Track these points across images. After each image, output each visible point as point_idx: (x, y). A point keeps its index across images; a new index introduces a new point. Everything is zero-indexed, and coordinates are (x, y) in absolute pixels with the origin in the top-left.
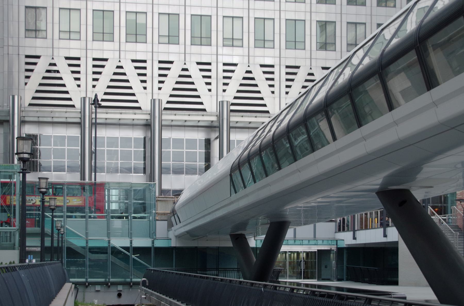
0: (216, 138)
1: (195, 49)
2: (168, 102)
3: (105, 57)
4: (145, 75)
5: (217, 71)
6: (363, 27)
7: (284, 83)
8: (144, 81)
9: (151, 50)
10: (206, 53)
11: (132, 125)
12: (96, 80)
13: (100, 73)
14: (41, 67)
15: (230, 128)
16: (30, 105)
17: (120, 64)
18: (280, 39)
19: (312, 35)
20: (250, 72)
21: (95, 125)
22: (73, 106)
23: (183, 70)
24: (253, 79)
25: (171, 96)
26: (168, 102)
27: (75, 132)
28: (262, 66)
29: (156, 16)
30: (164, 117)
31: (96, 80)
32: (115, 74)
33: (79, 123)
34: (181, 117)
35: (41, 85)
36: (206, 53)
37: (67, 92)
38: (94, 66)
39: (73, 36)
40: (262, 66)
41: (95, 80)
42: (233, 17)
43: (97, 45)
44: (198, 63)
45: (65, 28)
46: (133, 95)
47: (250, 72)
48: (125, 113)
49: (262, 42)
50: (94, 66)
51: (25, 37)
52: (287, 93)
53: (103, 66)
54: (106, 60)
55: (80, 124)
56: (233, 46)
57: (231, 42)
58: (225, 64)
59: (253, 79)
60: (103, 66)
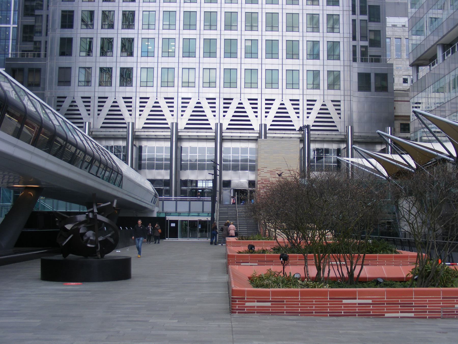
0: (345, 148)
1: (164, 89)
2: (271, 125)
3: (147, 96)
4: (215, 107)
5: (178, 103)
6: (193, 70)
7: (306, 111)
8: (256, 112)
9: (261, 93)
10: (170, 92)
11: (207, 139)
12: (268, 112)
13: (270, 108)
14: (150, 104)
15: (171, 139)
16: (227, 129)
17: (282, 102)
18: (220, 81)
19: (324, 80)
20: (199, 103)
21: (223, 140)
22: (211, 129)
23: (156, 103)
24: (201, 107)
25: (147, 119)
26: (271, 125)
27: (212, 145)
28: (207, 99)
29: (305, 72)
30: (169, 134)
31: (268, 112)
32: (154, 107)
33: (170, 139)
34: (236, 134)
35: (275, 117)
36: (170, 92)
37: (249, 121)
38: (266, 104)
39: (190, 85)
40: (207, 99)
41: (308, 113)
42: (189, 69)
43: (143, 89)
44: (165, 98)
45: (185, 80)
46: (291, 121)
47: (199, 103)
48: (156, 132)
49: (211, 84)
50: (266, 104)
51: (78, 86)
52: (224, 116)
53: (313, 105)
54: (148, 98)
55: (215, 139)
56: (188, 87)
57: (187, 84)
58: (183, 99)
59: (201, 107)
60: (230, 103)
